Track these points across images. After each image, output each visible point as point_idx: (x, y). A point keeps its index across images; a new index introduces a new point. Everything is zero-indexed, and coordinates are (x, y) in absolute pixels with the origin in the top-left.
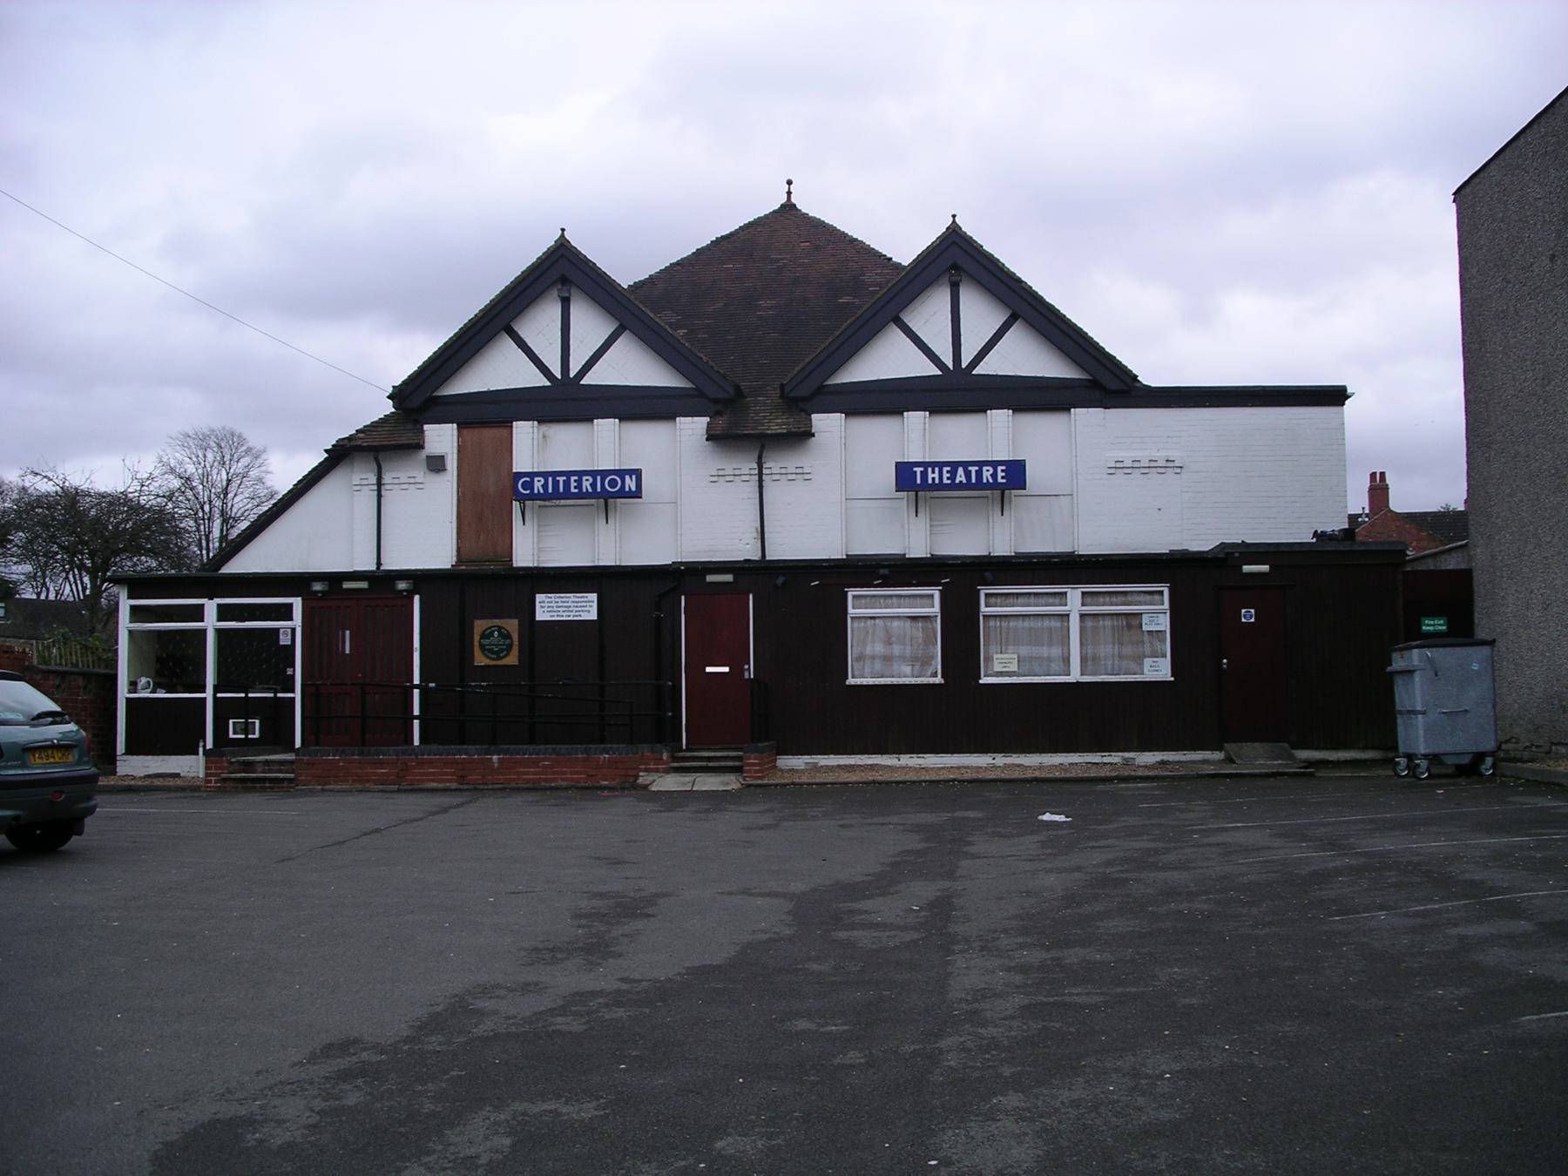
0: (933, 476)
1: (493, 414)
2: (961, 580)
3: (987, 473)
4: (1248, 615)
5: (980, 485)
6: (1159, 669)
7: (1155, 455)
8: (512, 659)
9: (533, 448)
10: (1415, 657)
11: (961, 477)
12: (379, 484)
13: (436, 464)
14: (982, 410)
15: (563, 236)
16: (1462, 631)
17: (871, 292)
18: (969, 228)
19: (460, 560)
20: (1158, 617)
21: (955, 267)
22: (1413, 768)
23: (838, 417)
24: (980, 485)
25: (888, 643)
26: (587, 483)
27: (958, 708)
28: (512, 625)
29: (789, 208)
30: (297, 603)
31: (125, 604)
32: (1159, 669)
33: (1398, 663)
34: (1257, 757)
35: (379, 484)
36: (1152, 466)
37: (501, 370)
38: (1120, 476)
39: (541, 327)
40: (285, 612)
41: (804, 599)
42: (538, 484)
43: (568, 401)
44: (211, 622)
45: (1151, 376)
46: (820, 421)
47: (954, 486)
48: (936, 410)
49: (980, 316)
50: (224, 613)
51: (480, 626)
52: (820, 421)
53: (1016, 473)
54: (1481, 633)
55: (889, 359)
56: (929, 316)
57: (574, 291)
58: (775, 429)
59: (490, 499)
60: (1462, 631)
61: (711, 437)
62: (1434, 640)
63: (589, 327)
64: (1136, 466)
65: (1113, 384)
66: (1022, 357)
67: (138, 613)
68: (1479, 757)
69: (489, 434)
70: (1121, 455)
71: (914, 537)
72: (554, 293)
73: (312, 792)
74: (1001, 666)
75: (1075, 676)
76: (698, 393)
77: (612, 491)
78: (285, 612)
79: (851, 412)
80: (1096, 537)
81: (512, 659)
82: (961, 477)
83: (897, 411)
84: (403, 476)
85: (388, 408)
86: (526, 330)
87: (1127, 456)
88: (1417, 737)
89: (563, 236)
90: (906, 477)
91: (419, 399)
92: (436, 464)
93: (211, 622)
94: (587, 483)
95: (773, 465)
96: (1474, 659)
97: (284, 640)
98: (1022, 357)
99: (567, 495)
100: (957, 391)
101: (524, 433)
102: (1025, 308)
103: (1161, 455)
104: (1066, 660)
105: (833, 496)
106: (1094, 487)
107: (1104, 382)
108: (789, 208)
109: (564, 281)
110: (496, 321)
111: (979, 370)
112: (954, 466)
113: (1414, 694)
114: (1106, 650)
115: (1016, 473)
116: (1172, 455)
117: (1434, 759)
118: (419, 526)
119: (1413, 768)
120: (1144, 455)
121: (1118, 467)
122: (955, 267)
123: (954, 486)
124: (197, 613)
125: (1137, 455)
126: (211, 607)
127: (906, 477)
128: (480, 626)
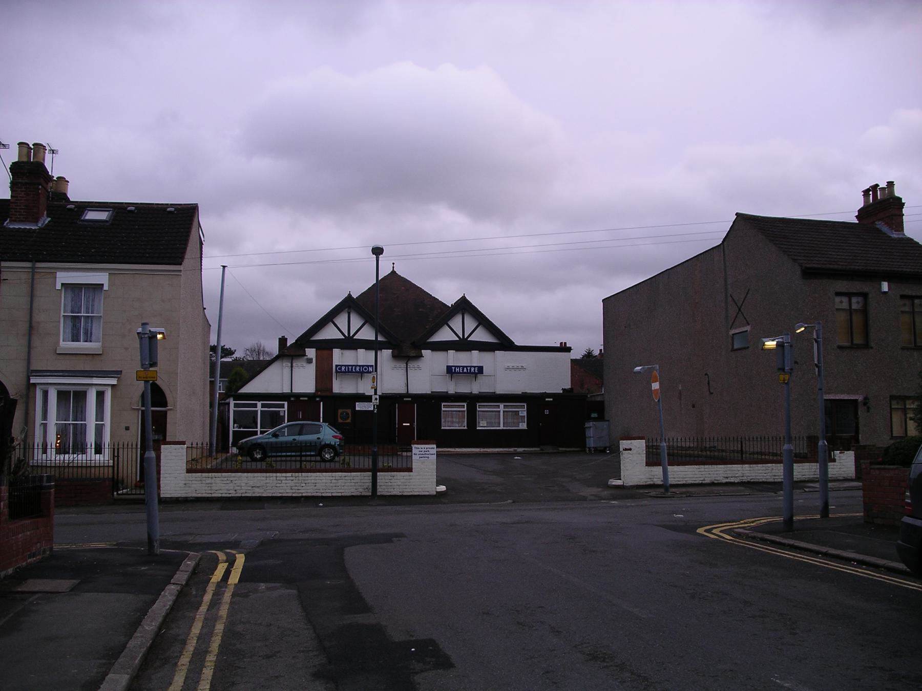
0: (457, 370)
1: (326, 347)
2: (472, 400)
3: (473, 369)
4: (547, 412)
5: (470, 373)
6: (523, 426)
8: (349, 421)
9: (339, 357)
10: (591, 424)
11: (465, 370)
12: (292, 367)
13: (310, 361)
14: (470, 350)
16: (601, 418)
17: (442, 314)
19: (316, 390)
20: (523, 413)
22: (590, 450)
24: (470, 373)
25: (453, 419)
26: (358, 369)
27: (471, 436)
28: (349, 411)
29: (393, 272)
30: (286, 403)
31: (232, 403)
32: (523, 426)
33: (587, 425)
34: (549, 449)
35: (292, 367)
36: (518, 368)
37: (329, 333)
38: (508, 371)
39: (342, 320)
40: (282, 406)
41: (431, 403)
42: (343, 368)
44: (259, 408)
45: (518, 342)
46: (425, 352)
47: (463, 373)
48: (457, 350)
49: (470, 324)
50: (263, 406)
51: (340, 411)
52: (425, 352)
53: (481, 369)
54: (606, 418)
55: (444, 335)
56: (456, 323)
58: (412, 354)
59: (324, 374)
60: (601, 418)
62: (595, 419)
64: (513, 368)
66: (481, 336)
67: (236, 405)
68: (606, 448)
69: (325, 352)
71: (452, 388)
74: (482, 425)
75: (502, 427)
77: (361, 371)
78: (282, 406)
79: (433, 350)
80: (503, 387)
81: (349, 421)
82: (465, 370)
87: (511, 365)
88: (591, 443)
90: (450, 370)
91: (305, 340)
92: (310, 361)
93: (259, 408)
94: (358, 369)
95: (411, 365)
96: (605, 424)
97: (282, 414)
98: (481, 336)
99: (352, 372)
100: (463, 345)
101: (336, 352)
102: (482, 321)
103: (520, 365)
104: (499, 423)
105: (427, 375)
106: (503, 374)
107: (504, 343)
108: (393, 272)
109: (349, 307)
112: (464, 367)
113: (590, 433)
114: (510, 420)
115: (481, 369)
117: (595, 448)
118: (304, 379)
119: (590, 450)
120: (515, 365)
121: (508, 368)
123: (463, 373)
124: (255, 406)
126: (259, 404)
127: (450, 370)
128: (340, 411)
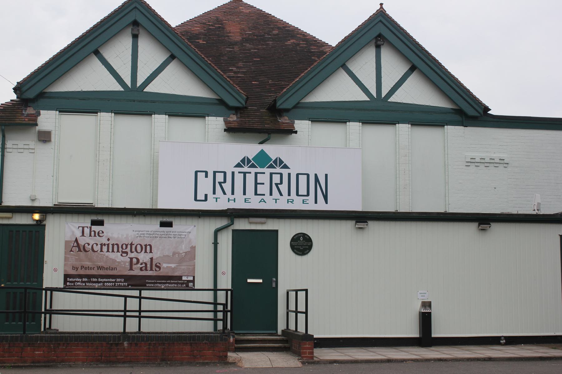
7: (493, 155)
15: (381, 7)
18: (390, 11)
21: (135, 24)
23: (307, 123)
38: (473, 167)
39: (119, 52)
43: (134, 101)
45: (494, 111)
49: (393, 67)
55: (338, 89)
57: (141, 31)
61: (230, 130)
63: (151, 55)
65: (471, 112)
66: (416, 93)
70: (473, 155)
72: (129, 31)
73: (95, 367)
76: (221, 102)
79: (314, 120)
83: (343, 121)
84: (21, 144)
85: (14, 97)
86: (110, 54)
87: (477, 155)
89: (381, 7)
98: (416, 93)
102: (421, 63)
103: (497, 156)
107: (468, 111)
110: (89, 45)
111: (392, 99)
116: (502, 156)
120: (487, 156)
121: (472, 162)
122: (135, 24)
125: (483, 155)
